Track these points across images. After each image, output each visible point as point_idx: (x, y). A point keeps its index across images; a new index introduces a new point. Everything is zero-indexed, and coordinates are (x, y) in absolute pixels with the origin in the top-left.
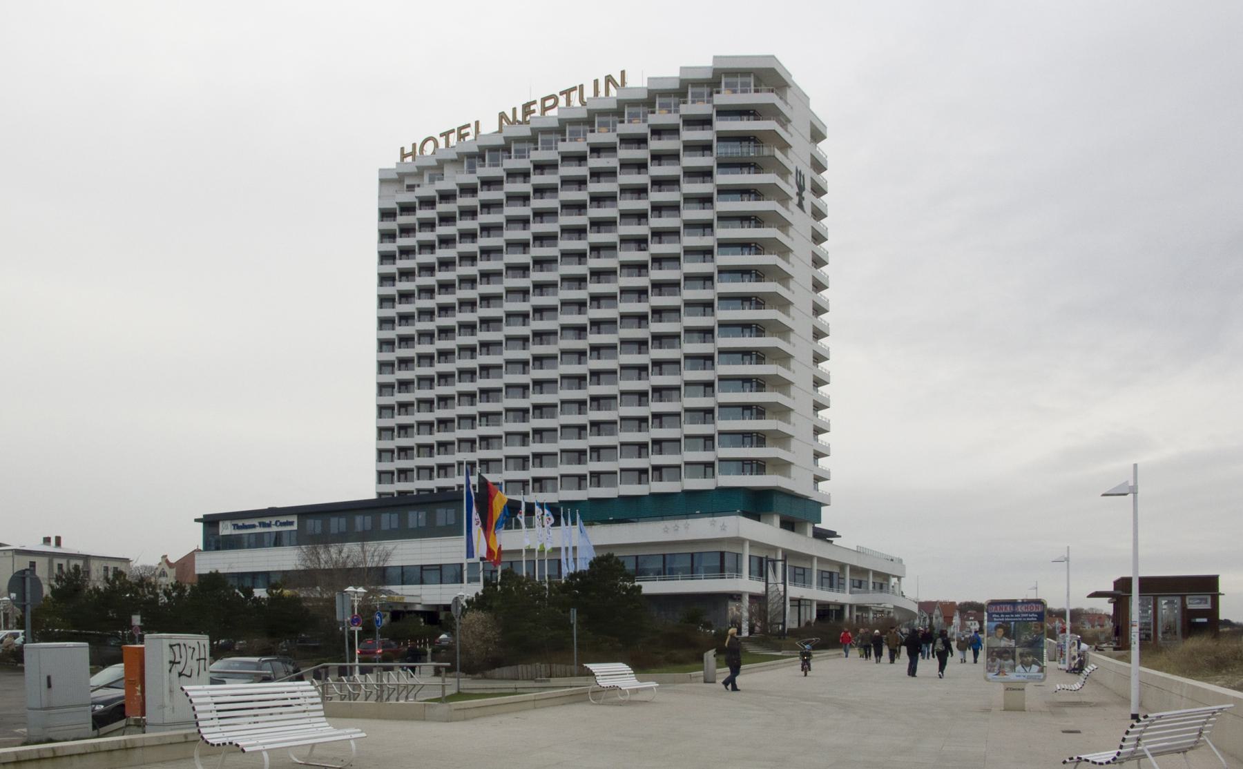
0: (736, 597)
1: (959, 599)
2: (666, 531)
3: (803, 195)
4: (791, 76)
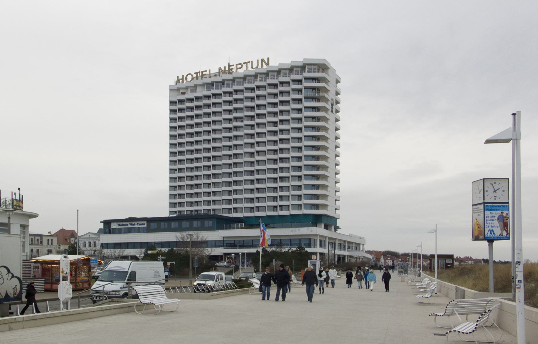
0: (315, 254)
1: (382, 249)
2: (292, 231)
4: (330, 64)
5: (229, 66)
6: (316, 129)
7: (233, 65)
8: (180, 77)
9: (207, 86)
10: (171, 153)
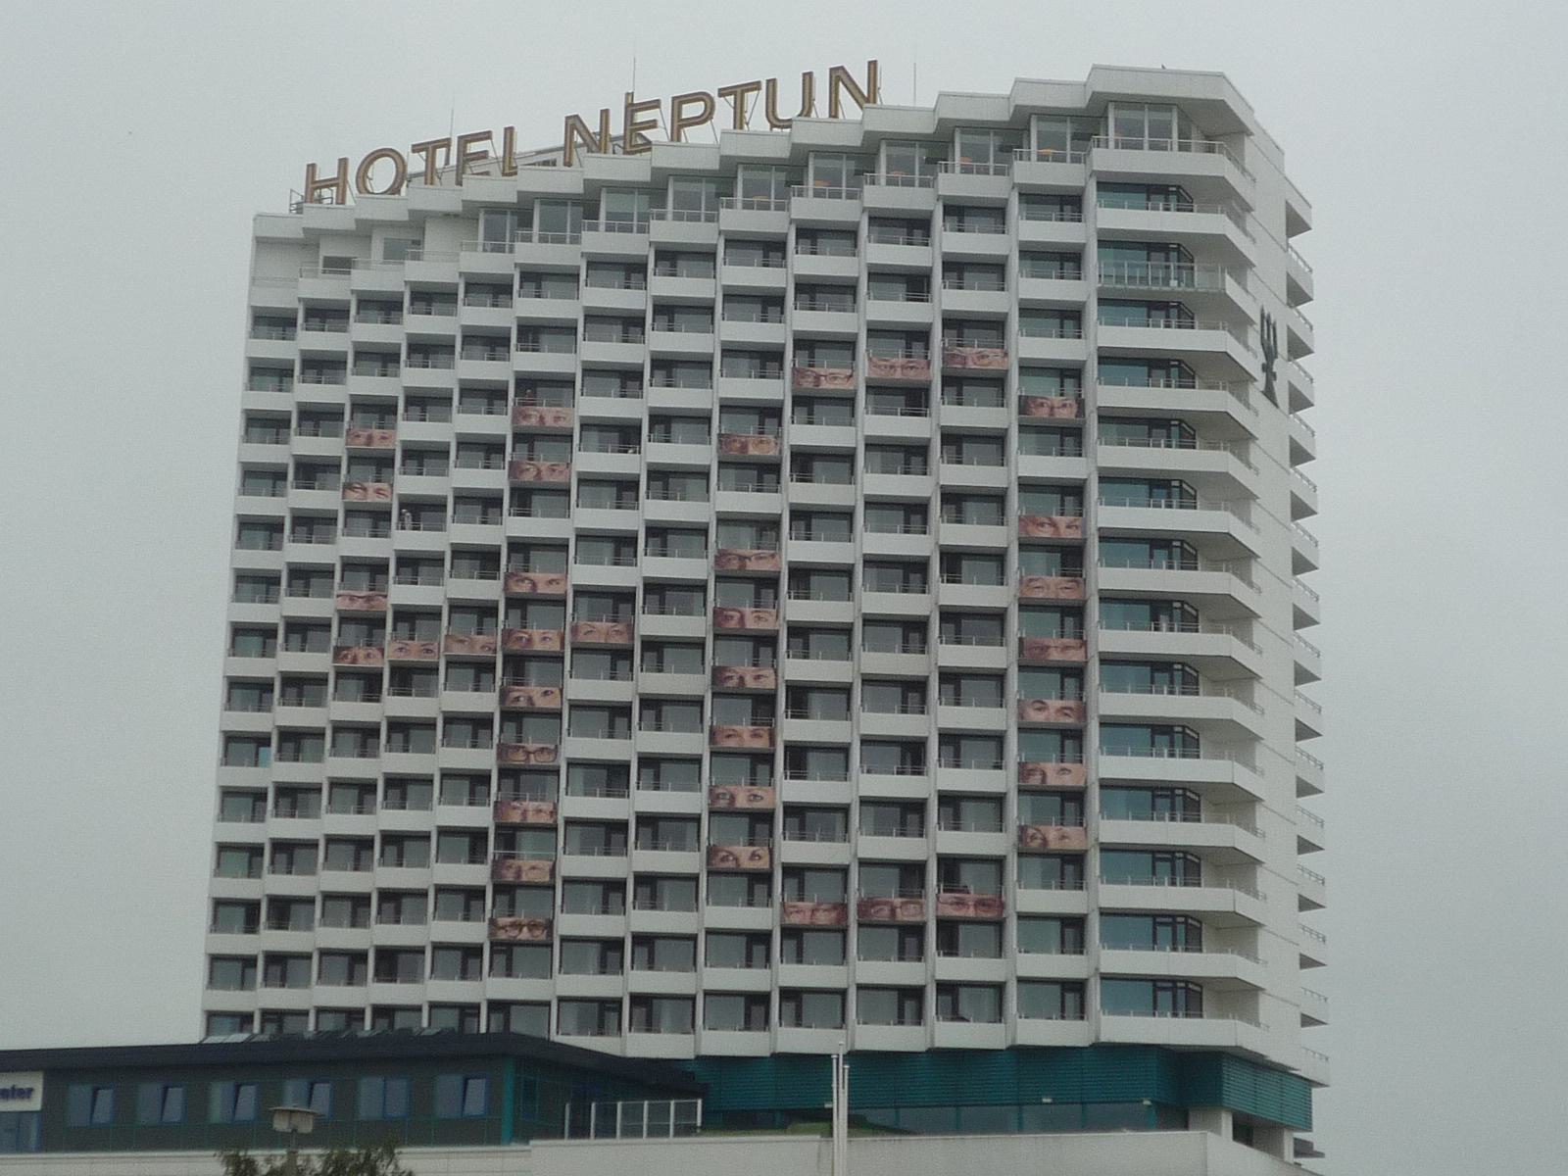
3: (1274, 370)
5: (632, 108)
6: (1177, 552)
7: (655, 104)
8: (328, 171)
9: (486, 220)
10: (235, 684)
